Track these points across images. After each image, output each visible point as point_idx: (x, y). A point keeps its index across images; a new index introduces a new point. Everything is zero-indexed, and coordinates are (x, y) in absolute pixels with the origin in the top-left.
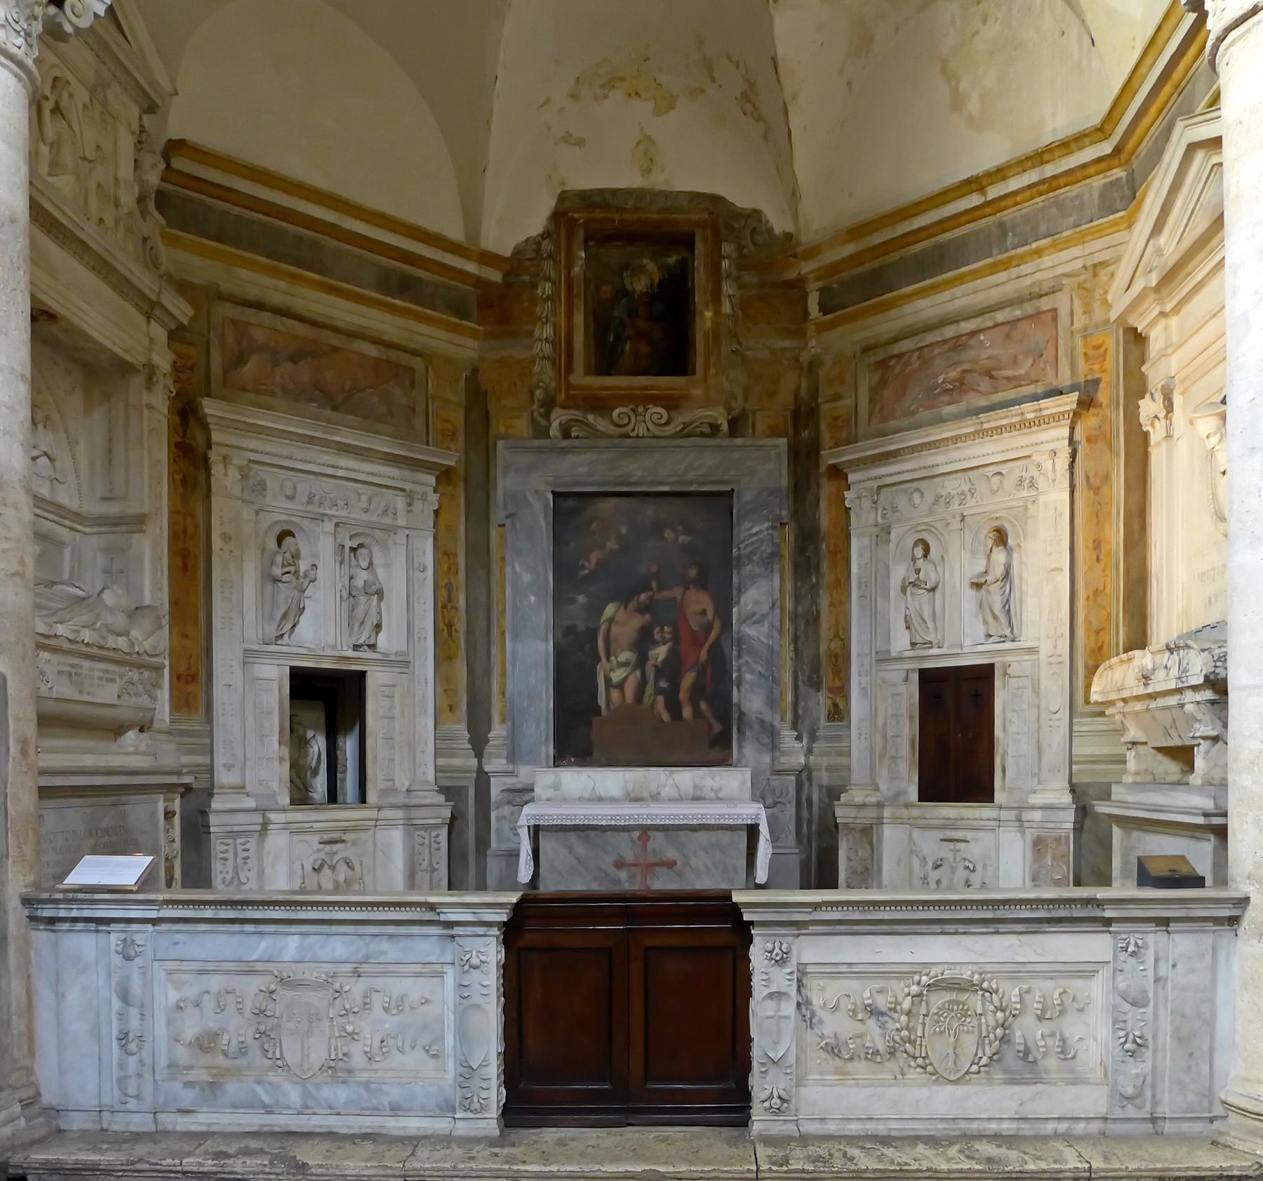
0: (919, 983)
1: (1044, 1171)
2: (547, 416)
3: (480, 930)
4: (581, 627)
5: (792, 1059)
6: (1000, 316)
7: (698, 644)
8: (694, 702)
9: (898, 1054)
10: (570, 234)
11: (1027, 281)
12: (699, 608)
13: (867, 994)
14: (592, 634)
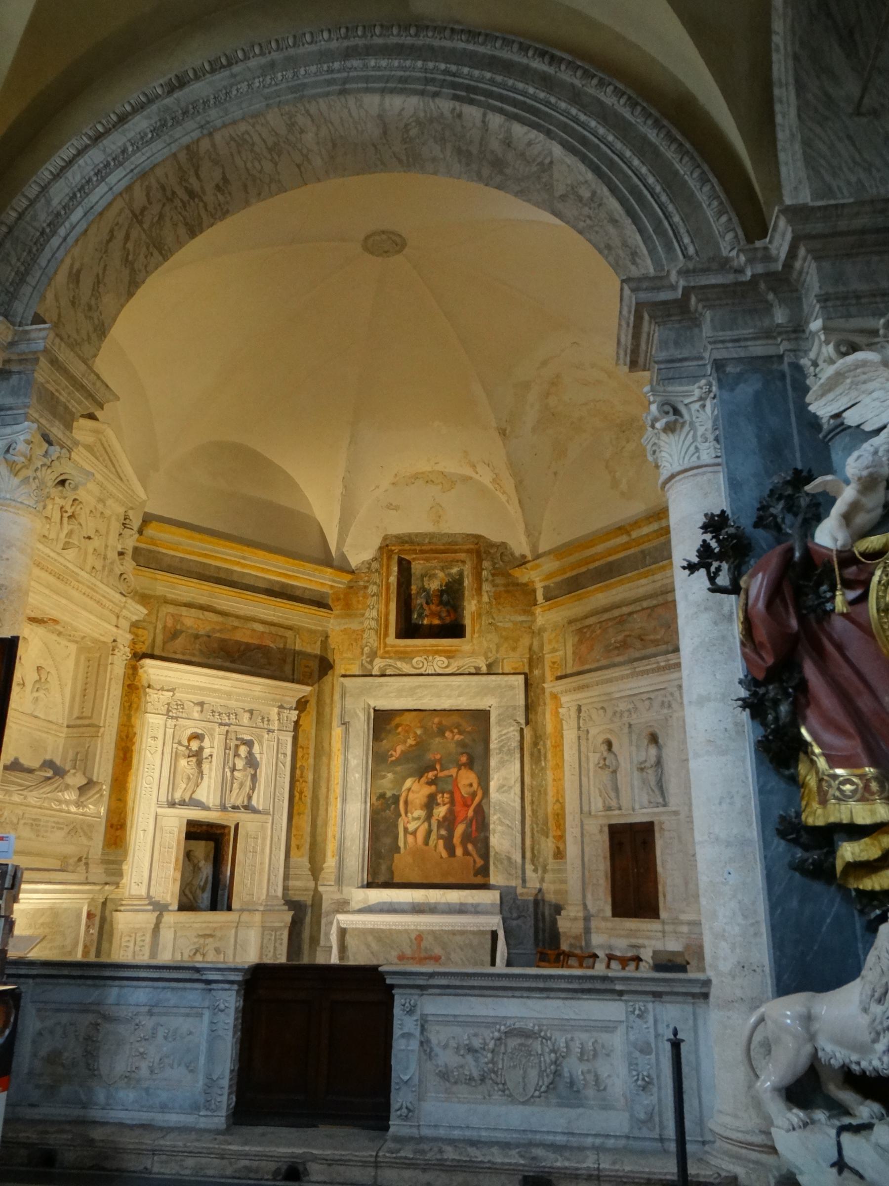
0: (499, 1031)
1: (566, 1168)
2: (371, 662)
3: (227, 986)
4: (389, 794)
5: (416, 1080)
6: (645, 604)
7: (467, 806)
8: (464, 843)
9: (487, 1080)
10: (389, 558)
11: (659, 584)
12: (467, 782)
13: (466, 1037)
14: (396, 798)
